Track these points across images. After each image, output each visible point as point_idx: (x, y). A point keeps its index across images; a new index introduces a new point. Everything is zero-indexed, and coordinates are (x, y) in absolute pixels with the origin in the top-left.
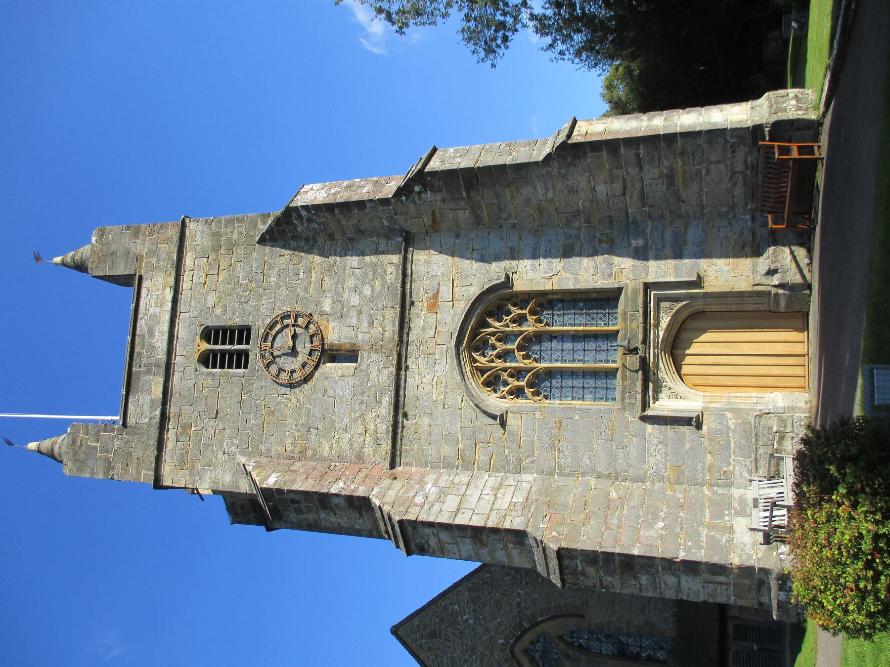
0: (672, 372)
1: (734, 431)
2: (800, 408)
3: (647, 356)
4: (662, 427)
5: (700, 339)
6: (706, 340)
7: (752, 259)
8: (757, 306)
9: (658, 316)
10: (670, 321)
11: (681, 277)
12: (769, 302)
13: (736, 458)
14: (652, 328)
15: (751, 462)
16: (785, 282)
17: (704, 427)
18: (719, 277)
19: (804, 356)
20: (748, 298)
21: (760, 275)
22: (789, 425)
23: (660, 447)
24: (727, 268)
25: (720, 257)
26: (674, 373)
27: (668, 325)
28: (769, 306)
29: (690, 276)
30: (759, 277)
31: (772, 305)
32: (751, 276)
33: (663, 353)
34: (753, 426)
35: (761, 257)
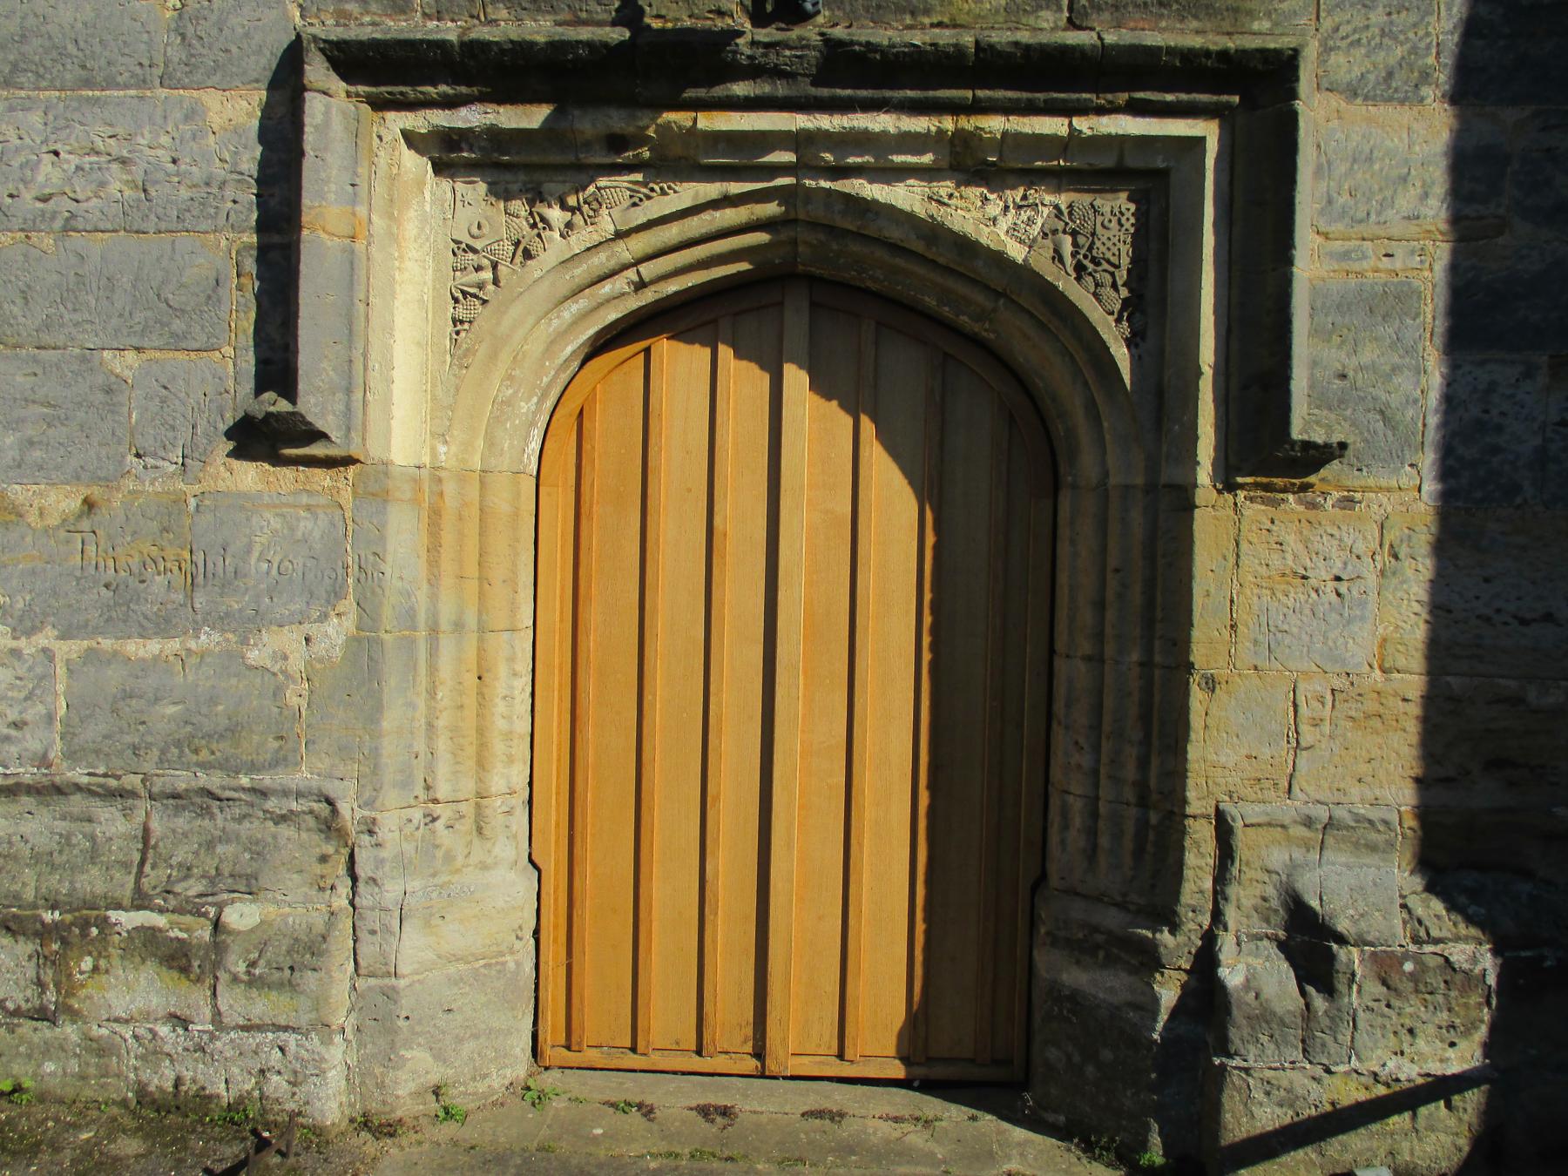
0: (648, 270)
1: (232, 661)
2: (390, 1059)
3: (740, 89)
4: (249, 196)
5: (877, 459)
6: (869, 495)
7: (1411, 822)
8: (1077, 821)
9: (1031, 177)
10: (999, 259)
11: (1315, 332)
12: (1098, 898)
13: (61, 671)
14: (948, 124)
15: (44, 761)
16: (1233, 1033)
17: (250, 475)
18: (1297, 594)
19: (759, 1054)
20: (1130, 772)
21: (1293, 866)
22: (262, 1006)
23: (114, 188)
24: (1359, 648)
25: (1440, 609)
26: (641, 285)
27: (966, 246)
28: (1073, 893)
29: (1319, 398)
30: (1278, 857)
31: (1078, 910)
32: (1288, 810)
33: (771, 209)
34: (266, 780)
35: (1417, 882)
